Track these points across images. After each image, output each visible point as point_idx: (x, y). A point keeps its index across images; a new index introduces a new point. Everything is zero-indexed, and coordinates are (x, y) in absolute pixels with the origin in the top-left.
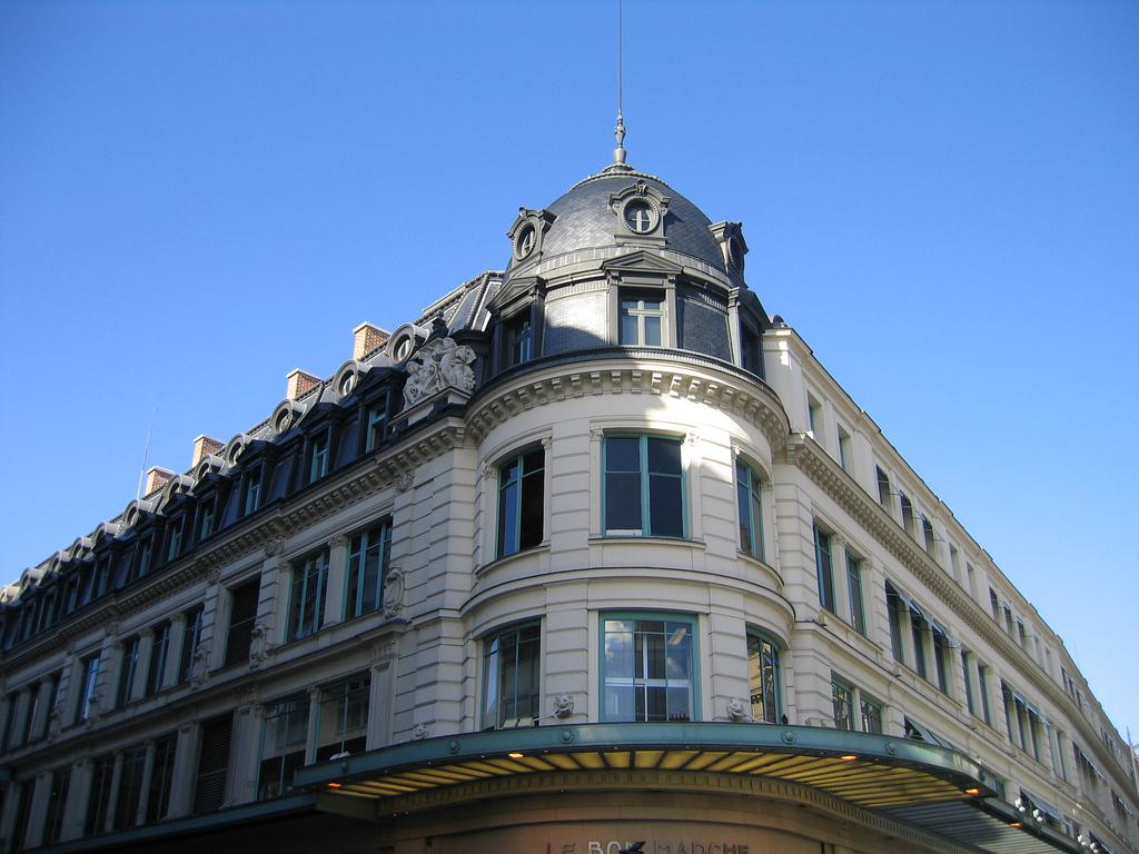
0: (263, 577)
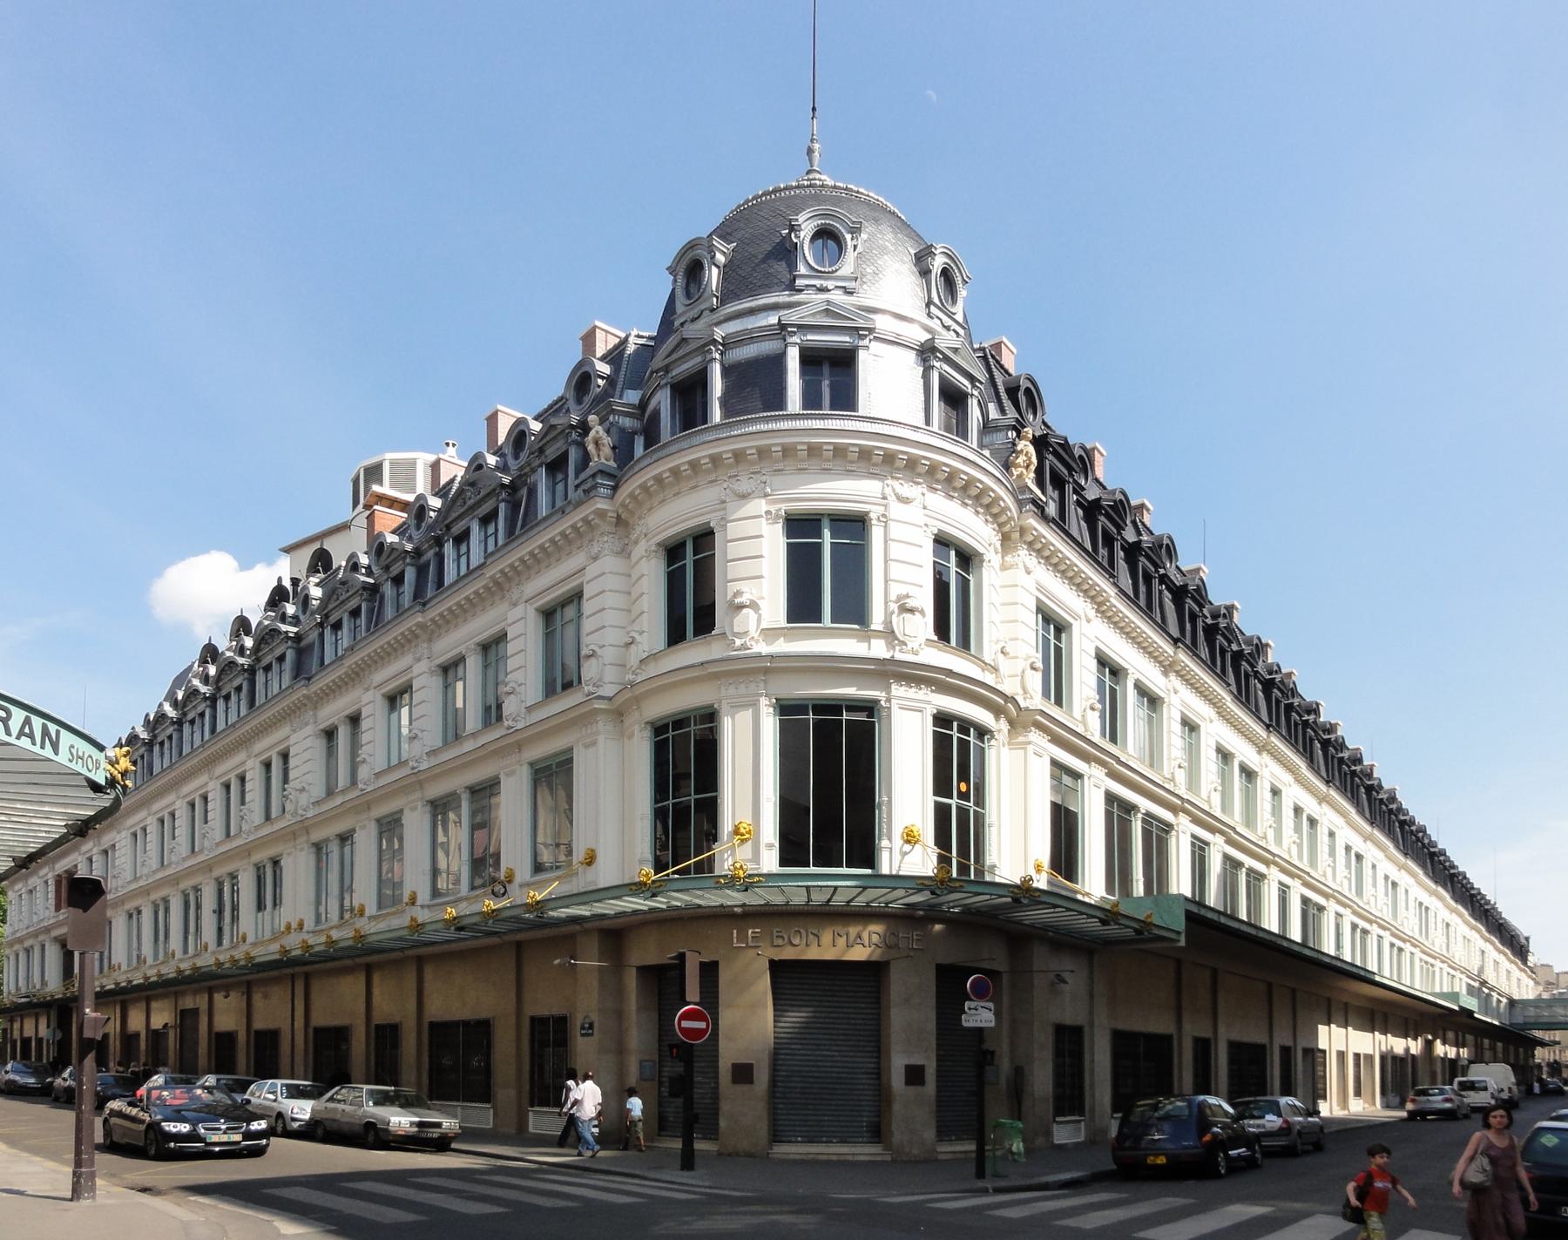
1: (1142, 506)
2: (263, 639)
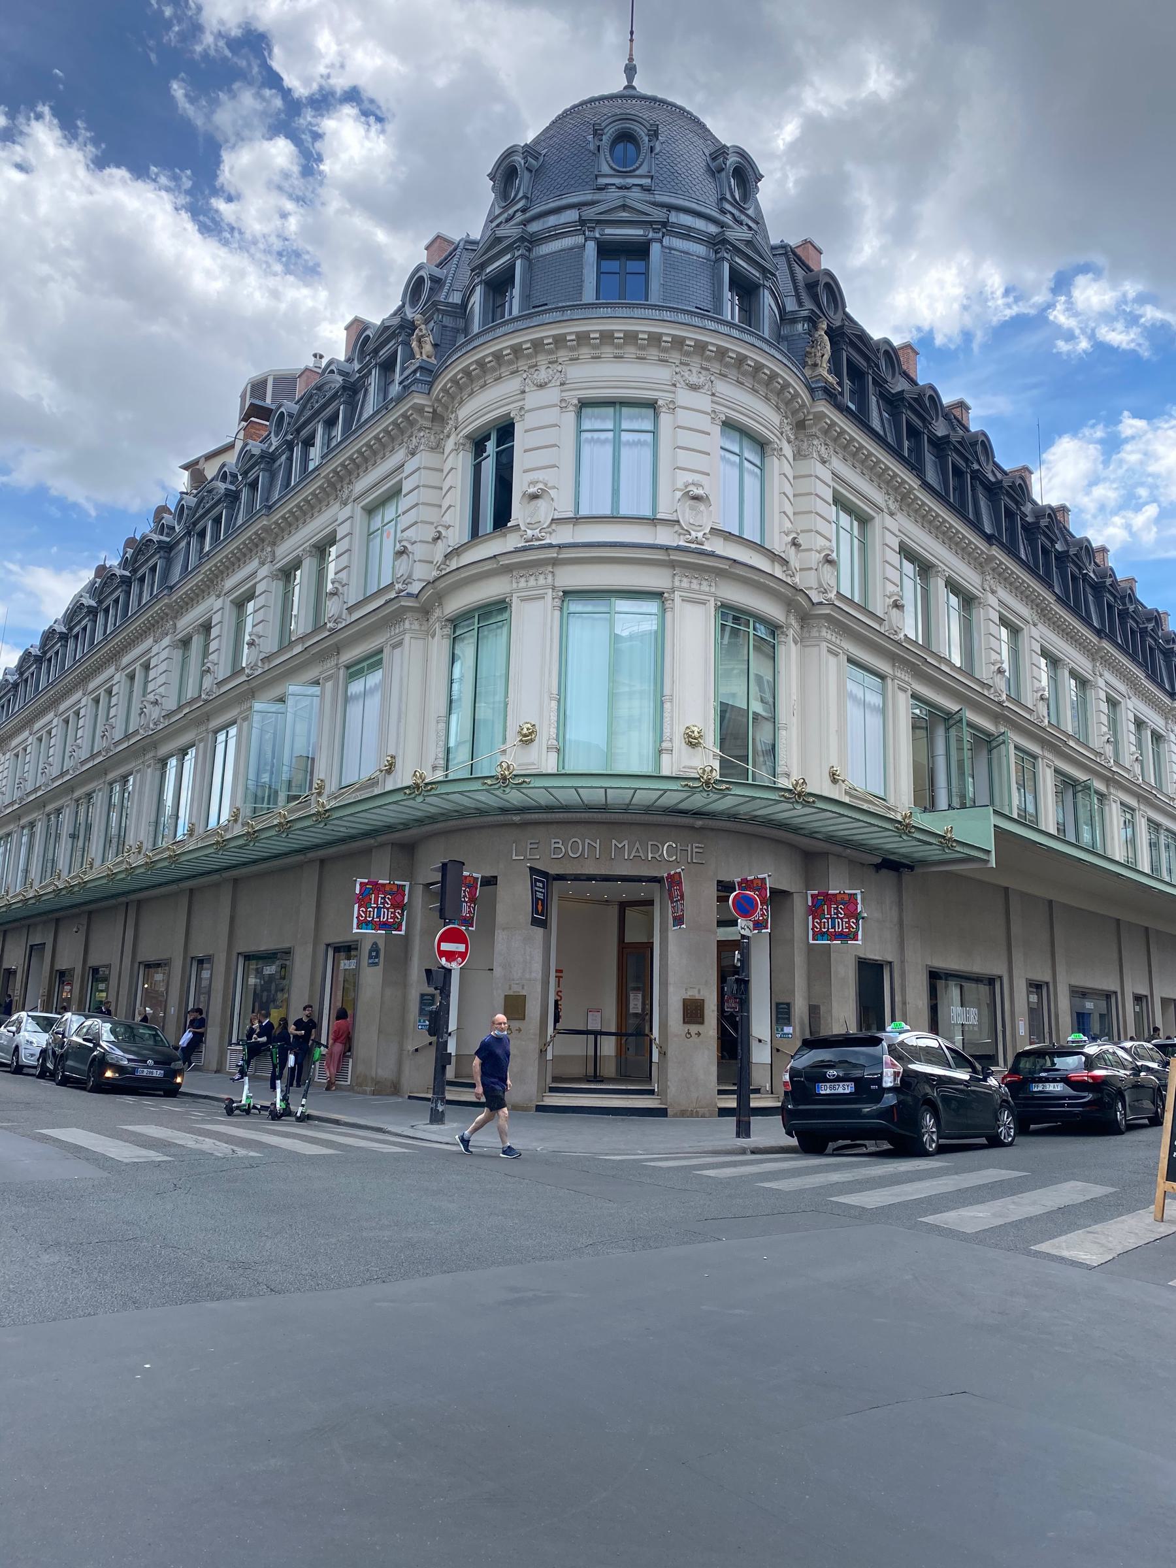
0: (338, 529)
1: (962, 405)
2: (140, 550)
